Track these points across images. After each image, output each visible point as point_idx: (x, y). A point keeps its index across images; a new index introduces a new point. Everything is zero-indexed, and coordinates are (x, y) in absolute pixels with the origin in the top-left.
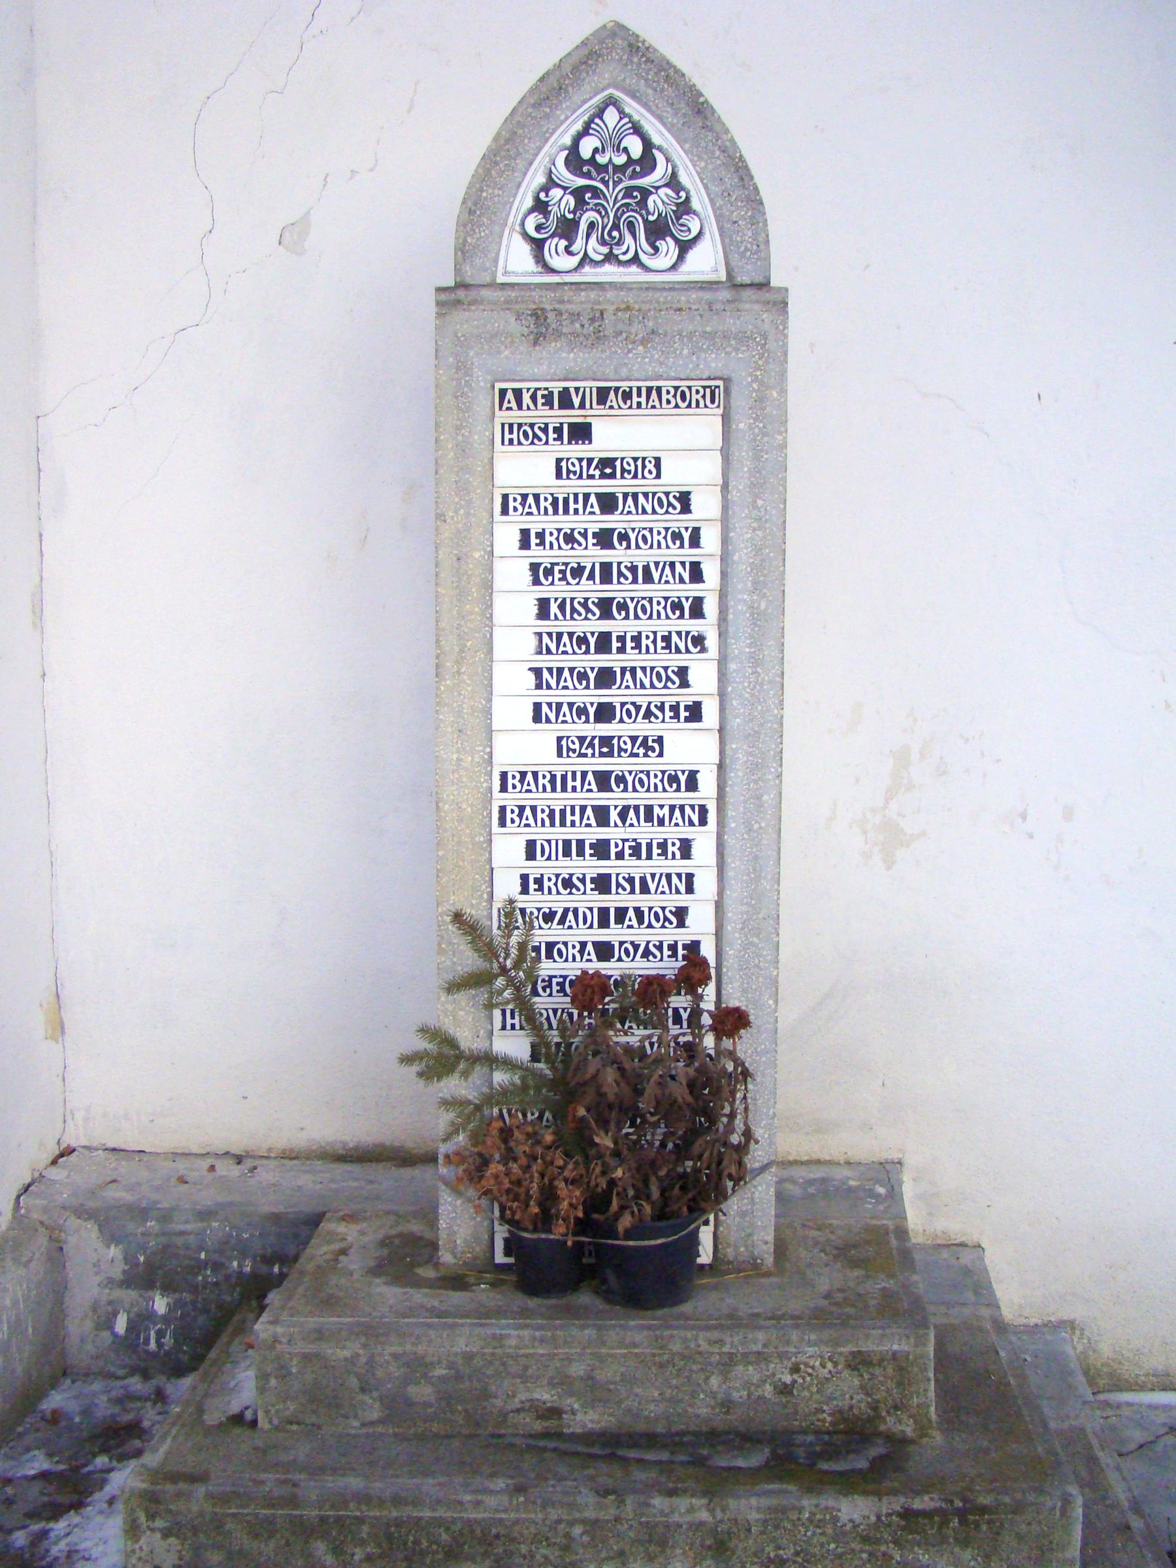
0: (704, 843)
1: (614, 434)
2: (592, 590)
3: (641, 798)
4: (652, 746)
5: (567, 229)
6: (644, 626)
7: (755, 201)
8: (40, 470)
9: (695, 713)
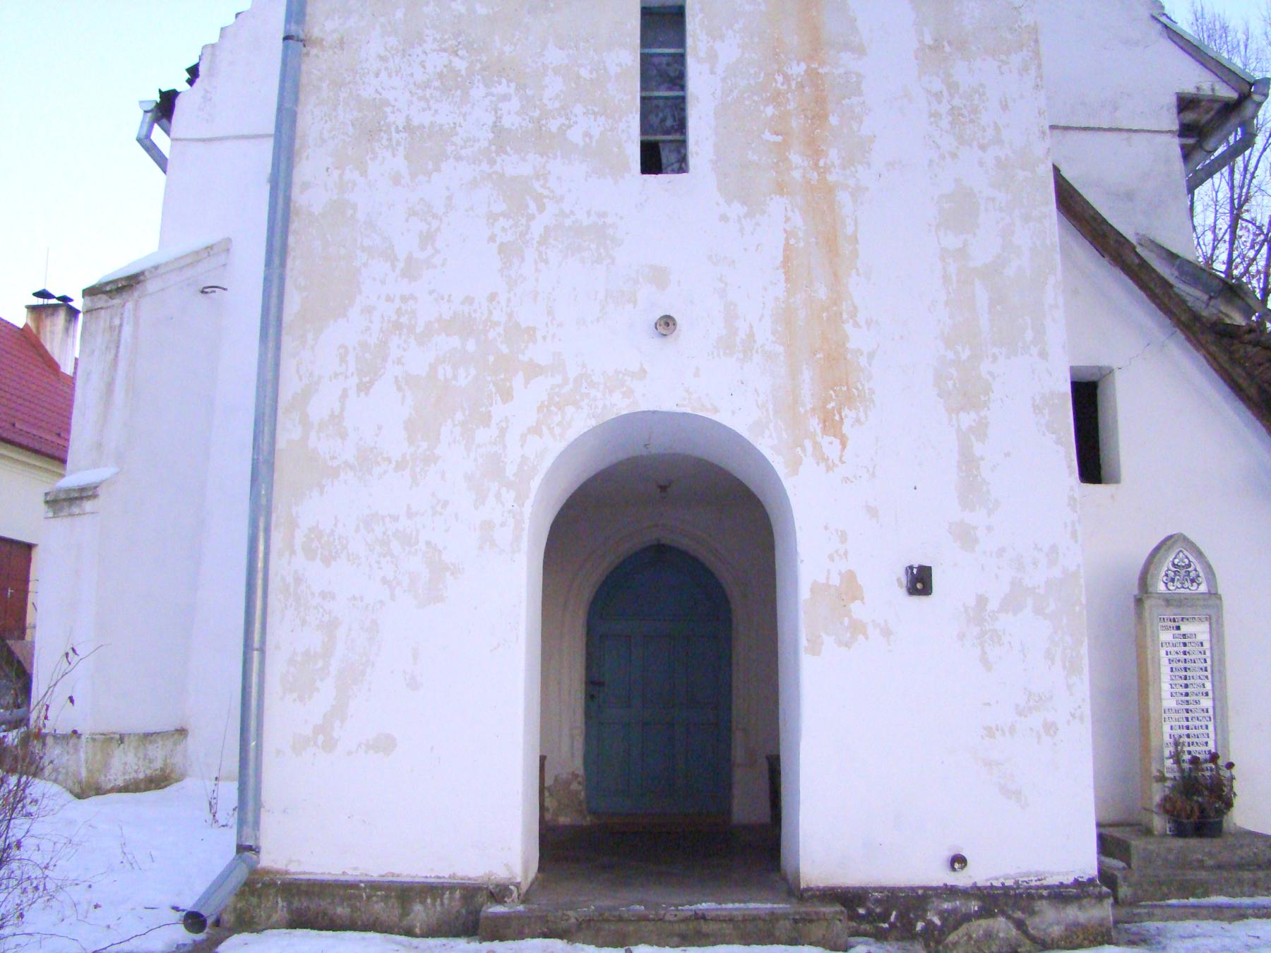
1: (1186, 628)
2: (1182, 665)
3: (1196, 715)
5: (1173, 580)
6: (1194, 674)
7: (1213, 574)
9: (1207, 694)
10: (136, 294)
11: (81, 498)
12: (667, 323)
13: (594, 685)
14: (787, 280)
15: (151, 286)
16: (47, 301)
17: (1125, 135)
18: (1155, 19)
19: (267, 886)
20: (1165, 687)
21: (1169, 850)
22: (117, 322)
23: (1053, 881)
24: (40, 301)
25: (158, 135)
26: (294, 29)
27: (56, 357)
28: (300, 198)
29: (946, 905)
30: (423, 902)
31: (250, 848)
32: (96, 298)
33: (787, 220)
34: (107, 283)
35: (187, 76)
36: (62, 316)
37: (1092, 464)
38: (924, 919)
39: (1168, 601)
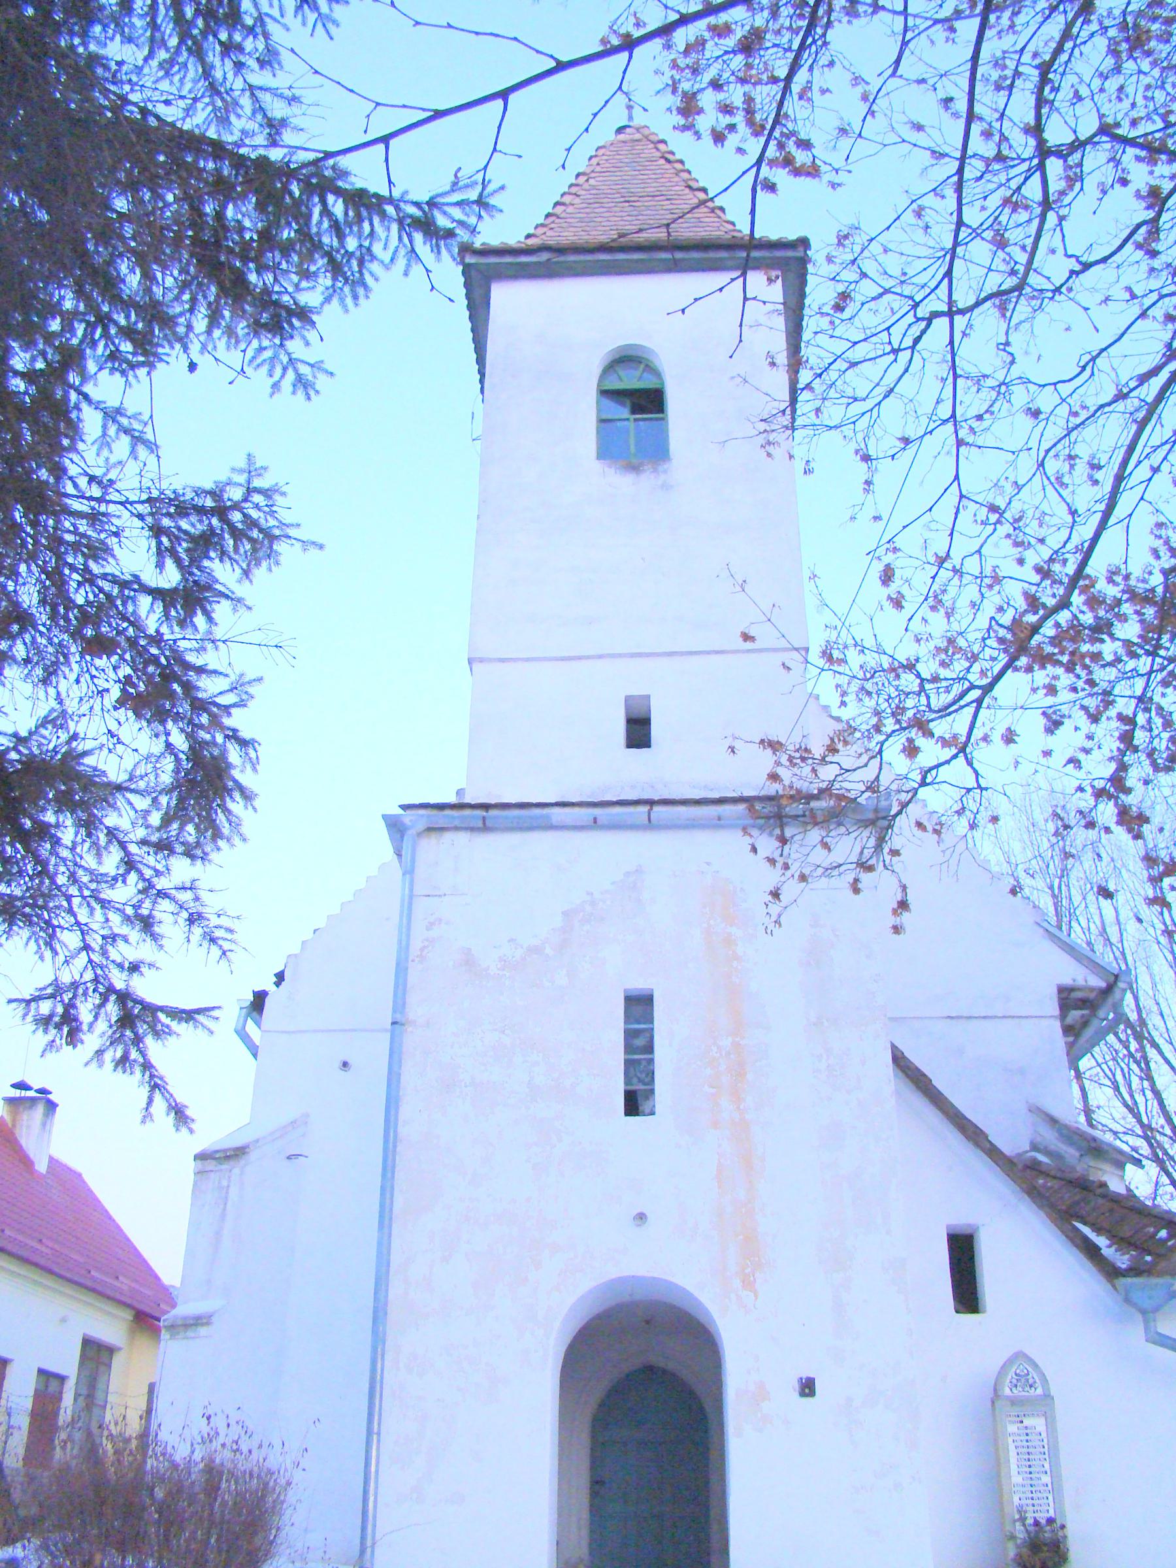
0: (1051, 1498)
1: (1027, 1422)
2: (1026, 1450)
4: (1040, 1479)
5: (1016, 1386)
8: (721, 290)
10: (242, 1162)
11: (196, 1325)
12: (641, 1217)
13: (597, 1484)
14: (719, 1187)
15: (253, 1155)
16: (24, 1093)
17: (1017, 1020)
18: (1038, 924)
20: (1014, 1468)
22: (225, 1183)
24: (17, 1093)
26: (398, 1017)
27: (31, 1154)
28: (403, 1131)
33: (720, 1146)
34: (217, 1151)
35: (275, 979)
36: (40, 1109)
37: (967, 1295)
39: (1014, 1402)
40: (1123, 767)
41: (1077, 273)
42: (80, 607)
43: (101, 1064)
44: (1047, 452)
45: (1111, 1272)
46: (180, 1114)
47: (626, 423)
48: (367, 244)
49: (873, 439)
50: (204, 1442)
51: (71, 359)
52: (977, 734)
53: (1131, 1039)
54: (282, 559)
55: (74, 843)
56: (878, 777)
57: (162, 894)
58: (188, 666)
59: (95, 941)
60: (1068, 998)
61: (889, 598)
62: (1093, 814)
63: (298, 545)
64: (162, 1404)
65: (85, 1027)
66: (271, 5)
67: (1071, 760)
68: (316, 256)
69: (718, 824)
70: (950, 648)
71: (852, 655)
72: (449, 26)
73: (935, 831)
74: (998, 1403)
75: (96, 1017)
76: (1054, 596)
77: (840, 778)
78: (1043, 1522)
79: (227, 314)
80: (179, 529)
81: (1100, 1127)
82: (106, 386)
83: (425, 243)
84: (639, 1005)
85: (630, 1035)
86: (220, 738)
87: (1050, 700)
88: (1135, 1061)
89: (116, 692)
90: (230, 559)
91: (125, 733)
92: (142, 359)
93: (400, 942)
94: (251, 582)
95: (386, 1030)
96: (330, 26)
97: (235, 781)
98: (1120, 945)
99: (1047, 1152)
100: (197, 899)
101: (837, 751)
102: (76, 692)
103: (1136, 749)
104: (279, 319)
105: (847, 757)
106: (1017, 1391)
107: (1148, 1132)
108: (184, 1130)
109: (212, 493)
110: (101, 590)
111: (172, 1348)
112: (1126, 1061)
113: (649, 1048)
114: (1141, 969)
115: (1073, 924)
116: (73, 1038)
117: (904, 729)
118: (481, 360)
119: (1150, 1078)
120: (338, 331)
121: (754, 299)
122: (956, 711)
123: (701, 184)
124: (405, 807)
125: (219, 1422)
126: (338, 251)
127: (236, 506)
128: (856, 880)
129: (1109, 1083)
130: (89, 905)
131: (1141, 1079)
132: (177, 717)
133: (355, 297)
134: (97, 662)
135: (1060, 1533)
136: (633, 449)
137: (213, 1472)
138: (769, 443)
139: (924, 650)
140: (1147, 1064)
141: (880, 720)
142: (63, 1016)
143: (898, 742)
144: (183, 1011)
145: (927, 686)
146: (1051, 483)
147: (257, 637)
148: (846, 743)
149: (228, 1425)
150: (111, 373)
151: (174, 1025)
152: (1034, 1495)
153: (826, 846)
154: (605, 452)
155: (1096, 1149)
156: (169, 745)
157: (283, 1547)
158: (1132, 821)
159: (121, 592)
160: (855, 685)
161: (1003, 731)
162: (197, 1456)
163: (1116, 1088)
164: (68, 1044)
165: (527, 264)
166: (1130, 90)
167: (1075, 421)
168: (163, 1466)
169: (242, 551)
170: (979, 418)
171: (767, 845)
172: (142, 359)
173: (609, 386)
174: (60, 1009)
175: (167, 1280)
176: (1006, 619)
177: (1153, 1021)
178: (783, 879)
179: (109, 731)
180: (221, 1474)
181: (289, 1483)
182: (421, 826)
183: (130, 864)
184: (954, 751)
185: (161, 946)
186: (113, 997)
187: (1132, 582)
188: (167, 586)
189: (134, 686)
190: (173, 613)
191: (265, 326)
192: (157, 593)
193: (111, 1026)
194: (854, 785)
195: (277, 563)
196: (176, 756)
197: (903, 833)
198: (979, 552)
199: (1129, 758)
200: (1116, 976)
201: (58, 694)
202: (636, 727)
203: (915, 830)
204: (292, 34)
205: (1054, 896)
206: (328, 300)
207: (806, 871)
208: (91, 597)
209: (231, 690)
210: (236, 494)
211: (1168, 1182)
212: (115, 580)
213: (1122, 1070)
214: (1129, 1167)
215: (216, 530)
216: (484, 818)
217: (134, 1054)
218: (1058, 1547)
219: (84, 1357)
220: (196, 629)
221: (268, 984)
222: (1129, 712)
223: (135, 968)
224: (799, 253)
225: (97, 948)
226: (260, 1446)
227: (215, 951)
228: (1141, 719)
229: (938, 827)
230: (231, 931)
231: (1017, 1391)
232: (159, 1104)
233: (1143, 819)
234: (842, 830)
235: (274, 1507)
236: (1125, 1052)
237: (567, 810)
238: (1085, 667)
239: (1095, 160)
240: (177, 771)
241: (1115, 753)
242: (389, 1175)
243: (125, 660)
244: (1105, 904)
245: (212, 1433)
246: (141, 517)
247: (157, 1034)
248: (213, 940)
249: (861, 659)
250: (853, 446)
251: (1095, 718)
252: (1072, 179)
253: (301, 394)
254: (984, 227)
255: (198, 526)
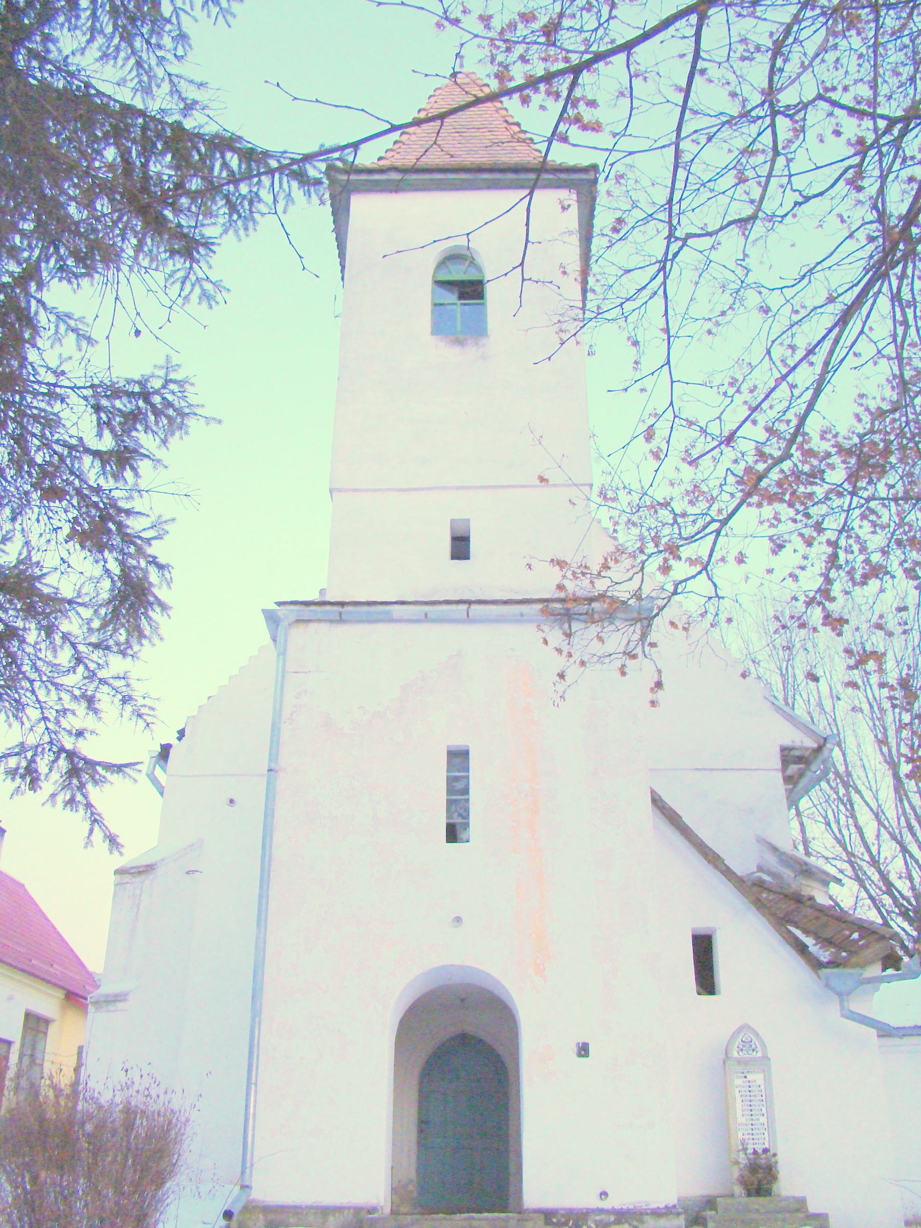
1: (750, 1077)
2: (748, 1098)
4: (758, 1120)
8: (506, 274)
10: (151, 876)
11: (115, 1001)
13: (423, 1124)
17: (749, 772)
18: (766, 698)
19: (255, 1207)
21: (740, 1203)
23: (653, 1206)
25: (159, 772)
26: (273, 766)
29: (597, 1218)
30: (334, 1215)
31: (247, 1186)
32: (123, 876)
38: (587, 1225)
39: (739, 1062)
40: (828, 581)
41: (800, 204)
42: (39, 465)
43: (54, 804)
44: (773, 342)
45: (816, 965)
46: (113, 841)
47: (454, 307)
48: (255, 189)
49: (641, 328)
50: (122, 1090)
51: (31, 274)
52: (717, 555)
53: (840, 786)
54: (190, 430)
55: (36, 643)
56: (640, 588)
57: (103, 681)
58: (120, 510)
59: (52, 715)
60: (788, 756)
61: (651, 451)
62: (804, 617)
63: (203, 420)
64: (90, 1061)
65: (42, 777)
66: (184, 3)
67: (792, 575)
68: (218, 198)
69: (520, 619)
70: (695, 492)
71: (622, 494)
72: (317, 101)
73: (685, 629)
74: (728, 1063)
75: (51, 770)
76: (779, 449)
77: (610, 589)
78: (760, 1151)
79: (149, 241)
80: (114, 407)
81: (815, 854)
82: (57, 294)
83: (299, 189)
84: (458, 758)
85: (450, 781)
86: (143, 564)
87: (772, 531)
88: (845, 805)
89: (67, 529)
90: (153, 431)
91: (72, 560)
92: (83, 271)
93: (274, 708)
94: (168, 449)
95: (262, 775)
96: (229, 17)
97: (156, 597)
98: (832, 714)
99: (769, 873)
100: (128, 685)
101: (609, 568)
102: (36, 529)
103: (840, 567)
104: (189, 247)
105: (617, 572)
106: (742, 1054)
107: (851, 859)
108: (116, 853)
109: (139, 383)
110: (55, 453)
111: (97, 1019)
112: (836, 803)
113: (466, 791)
114: (849, 733)
115: (797, 697)
116: (34, 784)
117: (661, 552)
118: (342, 255)
119: (853, 816)
120: (232, 254)
121: (530, 279)
122: (701, 538)
123: (516, 120)
124: (280, 604)
125: (134, 1074)
126: (234, 195)
127: (157, 392)
128: (623, 666)
129: (823, 821)
130: (46, 687)
131: (847, 817)
132: (112, 549)
133: (246, 229)
134: (52, 504)
135: (773, 1160)
136: (459, 328)
137: (129, 1112)
138: (561, 331)
139: (677, 492)
140: (852, 805)
141: (642, 544)
142: (26, 768)
143: (658, 560)
144: (114, 765)
145: (679, 520)
146: (777, 367)
147: (171, 488)
148: (617, 561)
149: (142, 1076)
150: (60, 279)
151: (108, 775)
152: (754, 1132)
153: (600, 639)
154: (437, 329)
155: (807, 871)
156: (107, 571)
157: (183, 1168)
158: (835, 623)
159: (70, 453)
160: (624, 518)
161: (736, 554)
162: (118, 1100)
163: (828, 824)
164: (30, 789)
165: (377, 181)
166: (844, 61)
167: (795, 318)
168: (92, 1108)
169: (161, 425)
170: (723, 314)
171: (556, 636)
172: (83, 271)
173: (442, 277)
174: (24, 764)
175: (91, 967)
176: (740, 469)
177: (857, 773)
178: (568, 664)
179: (62, 559)
180: (136, 1114)
181: (188, 1120)
182: (292, 618)
183: (79, 659)
184: (699, 568)
185: (100, 718)
186: (64, 755)
187: (840, 439)
188: (105, 449)
189: (80, 524)
190: (108, 468)
191: (178, 252)
192: (96, 454)
193: (62, 777)
194: (623, 592)
195: (187, 433)
196: (112, 578)
197: (660, 630)
198: (719, 418)
199: (833, 574)
200: (825, 739)
201: (23, 530)
202: (457, 543)
203: (669, 627)
204: (199, 25)
205: (781, 674)
206: (226, 232)
207: (585, 659)
208: (48, 459)
209: (152, 528)
210: (157, 384)
211: (867, 896)
212: (65, 445)
213: (833, 810)
214: (832, 884)
215: (140, 410)
216: (340, 613)
217: (79, 797)
218: (771, 1170)
219: (26, 1026)
220: (126, 482)
221: (172, 739)
222: (833, 539)
223: (80, 734)
224: (591, 176)
225: (52, 719)
226: (166, 1092)
227: (141, 723)
228: (842, 542)
229: (686, 626)
230: (152, 709)
231: (742, 1054)
232: (98, 834)
233: (842, 621)
234: (612, 627)
235: (176, 1138)
236: (835, 797)
237: (404, 607)
238: (803, 504)
239: (816, 116)
240: (112, 590)
241: (824, 571)
242: (265, 887)
243: (73, 506)
244: (812, 684)
245: (129, 1083)
246: (85, 398)
247: (96, 783)
248: (140, 715)
249: (629, 498)
250: (626, 334)
251: (809, 543)
252: (797, 131)
253: (205, 304)
254: (730, 167)
255: (128, 405)
